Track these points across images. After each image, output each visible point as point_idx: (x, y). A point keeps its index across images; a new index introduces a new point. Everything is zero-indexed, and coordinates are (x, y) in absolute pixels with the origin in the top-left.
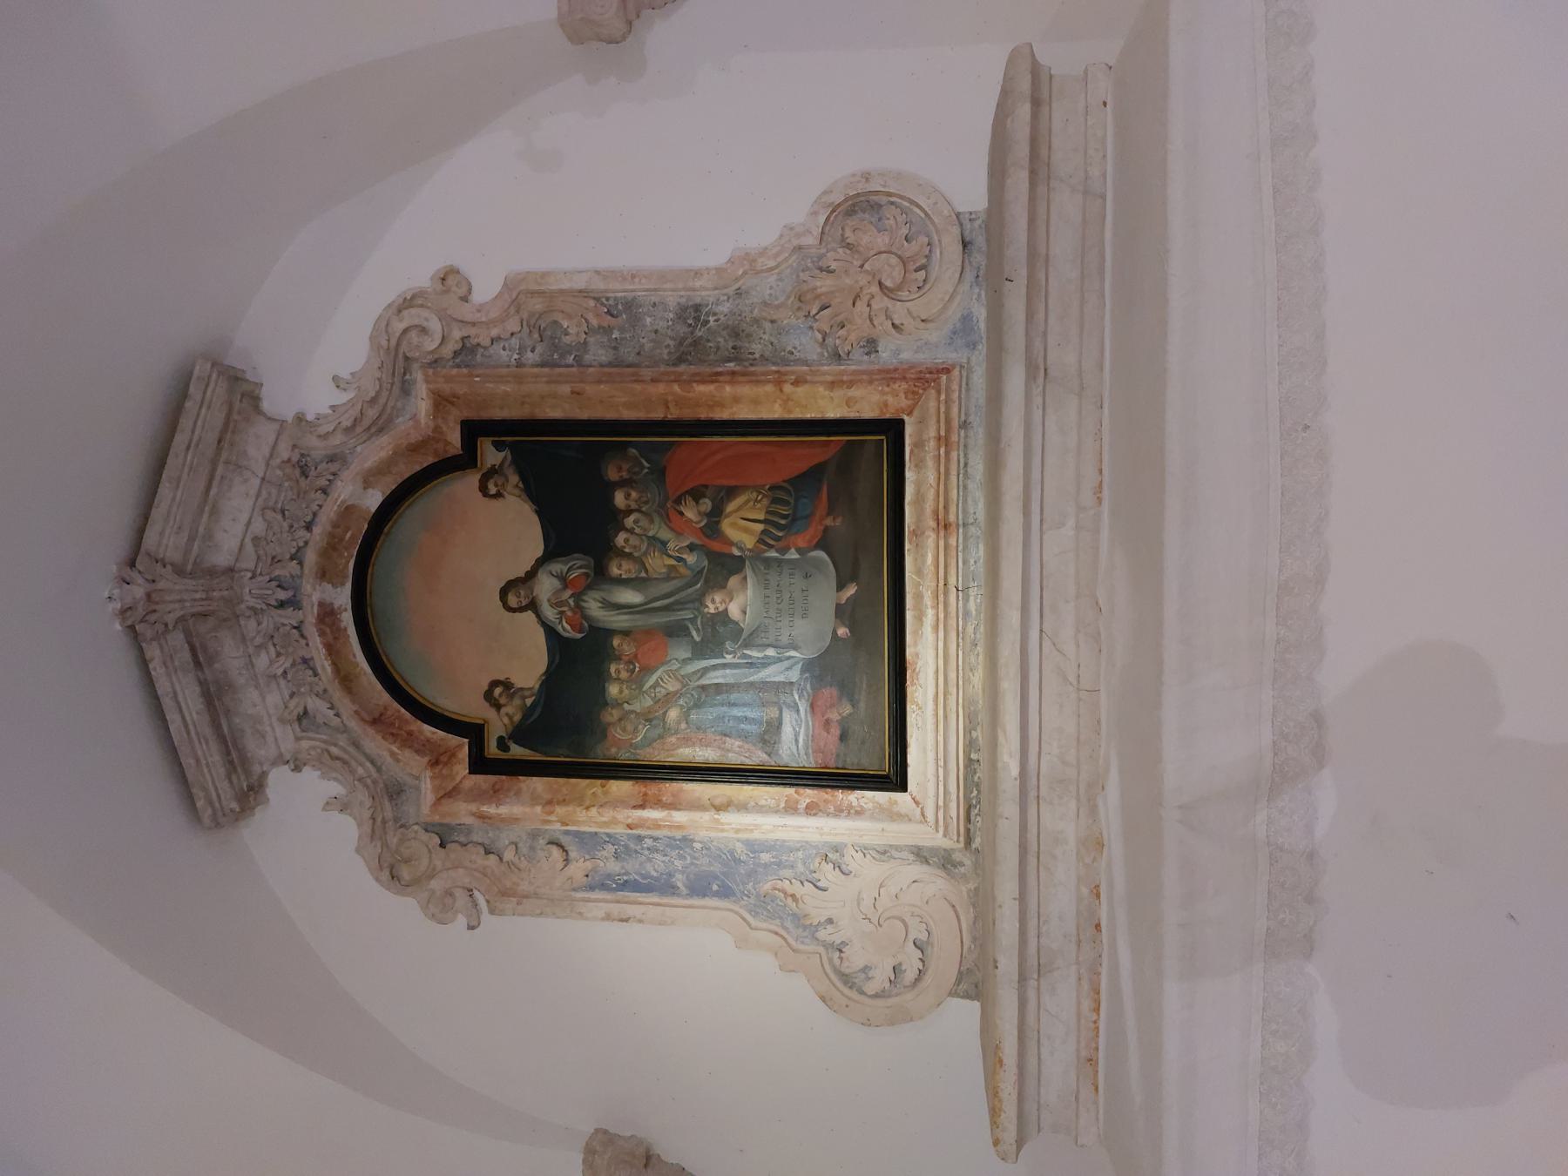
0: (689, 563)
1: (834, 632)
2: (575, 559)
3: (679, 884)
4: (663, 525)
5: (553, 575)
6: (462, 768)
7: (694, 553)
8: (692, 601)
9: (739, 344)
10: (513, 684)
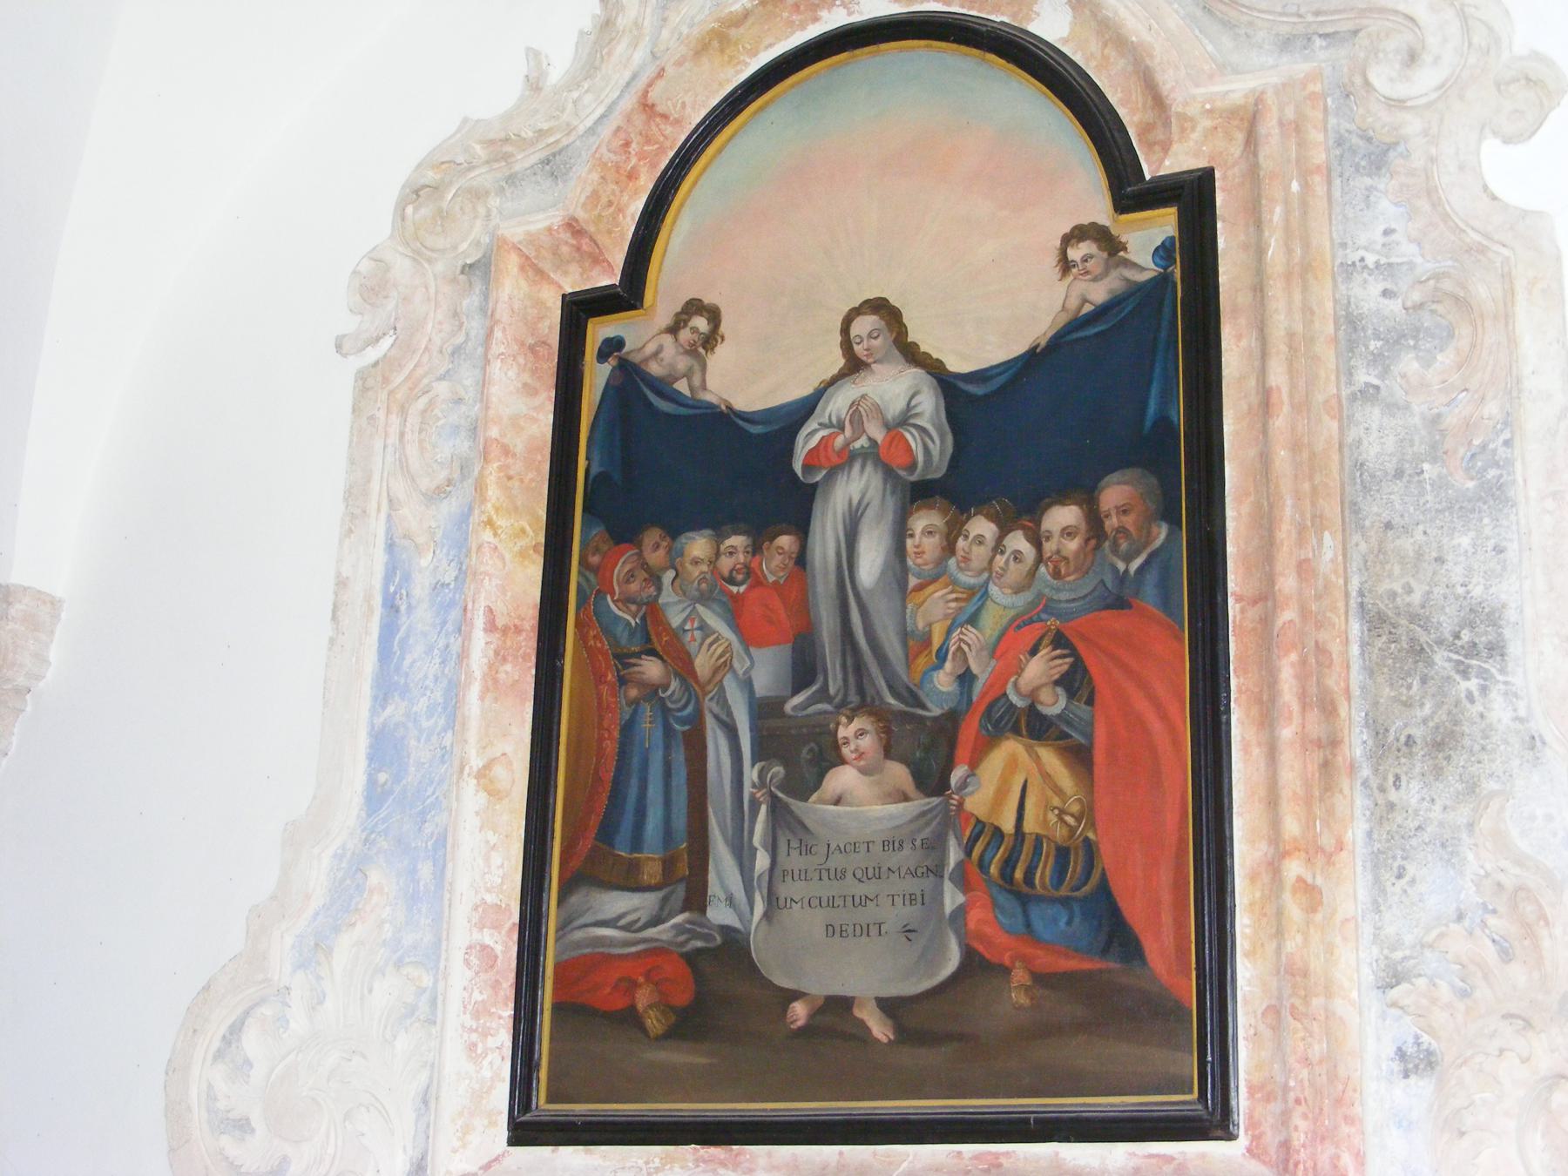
0: (935, 674)
1: (796, 995)
2: (943, 441)
3: (389, 710)
4: (1011, 613)
5: (912, 397)
6: (574, 282)
7: (955, 685)
8: (861, 691)
9: (1419, 751)
10: (712, 349)
